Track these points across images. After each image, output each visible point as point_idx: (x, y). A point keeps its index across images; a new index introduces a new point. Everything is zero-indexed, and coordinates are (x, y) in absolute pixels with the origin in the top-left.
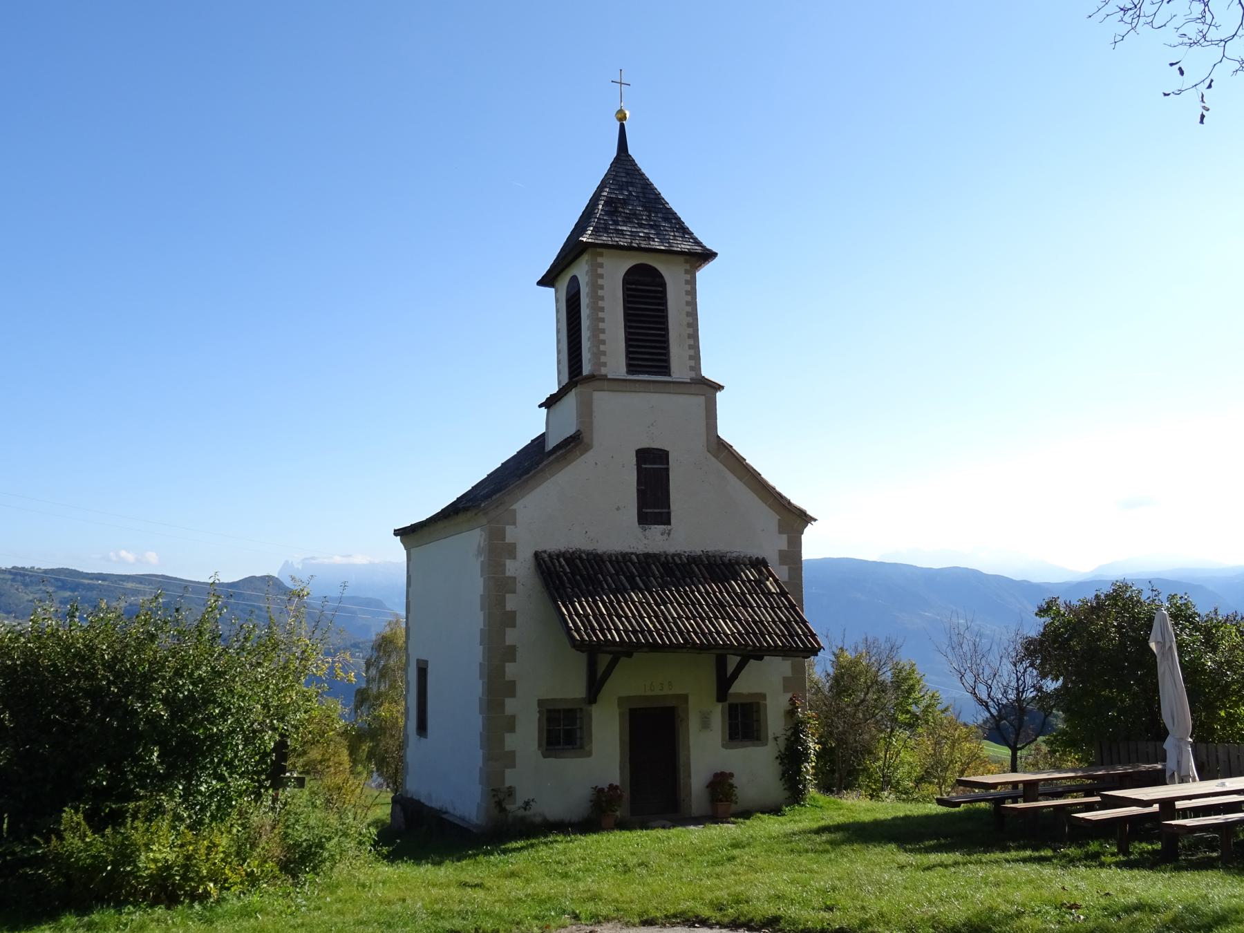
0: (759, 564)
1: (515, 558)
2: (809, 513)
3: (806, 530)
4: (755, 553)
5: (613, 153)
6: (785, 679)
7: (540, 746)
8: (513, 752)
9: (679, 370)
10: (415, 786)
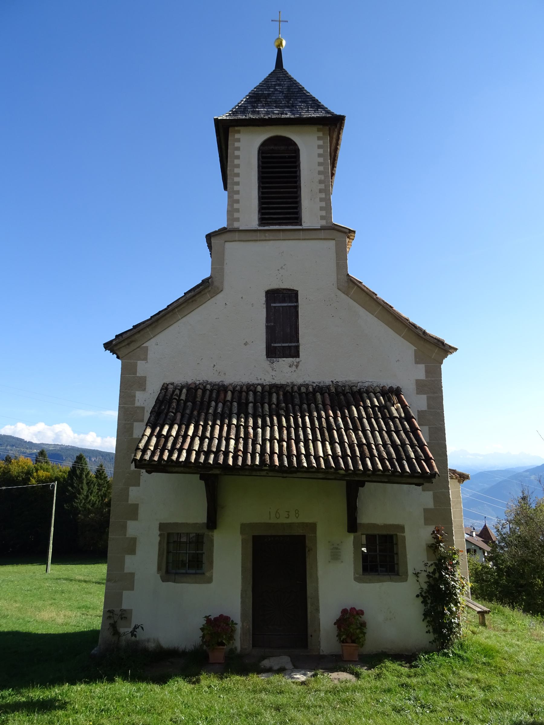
0: (392, 393)
1: (144, 390)
2: (448, 341)
3: (445, 361)
4: (388, 382)
5: (272, 67)
6: (426, 511)
7: (159, 569)
8: (132, 575)
9: (310, 217)
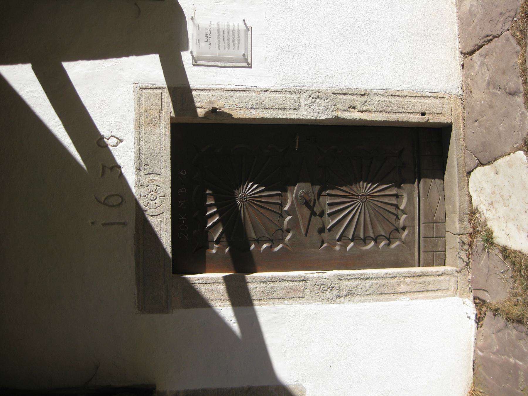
10: (213, 86)
